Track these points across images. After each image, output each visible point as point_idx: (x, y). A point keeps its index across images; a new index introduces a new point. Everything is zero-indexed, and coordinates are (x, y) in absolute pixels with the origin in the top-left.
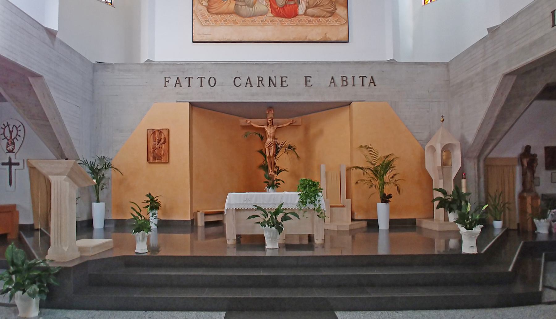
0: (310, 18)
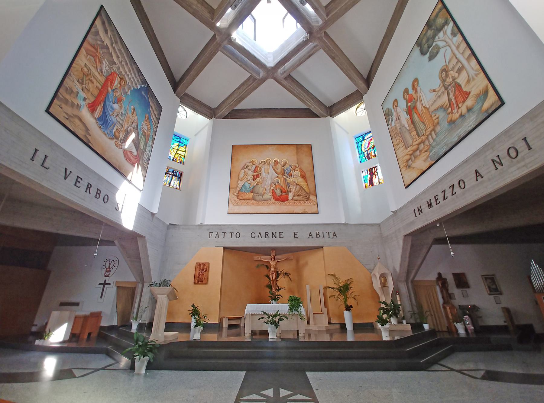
0: (295, 201)
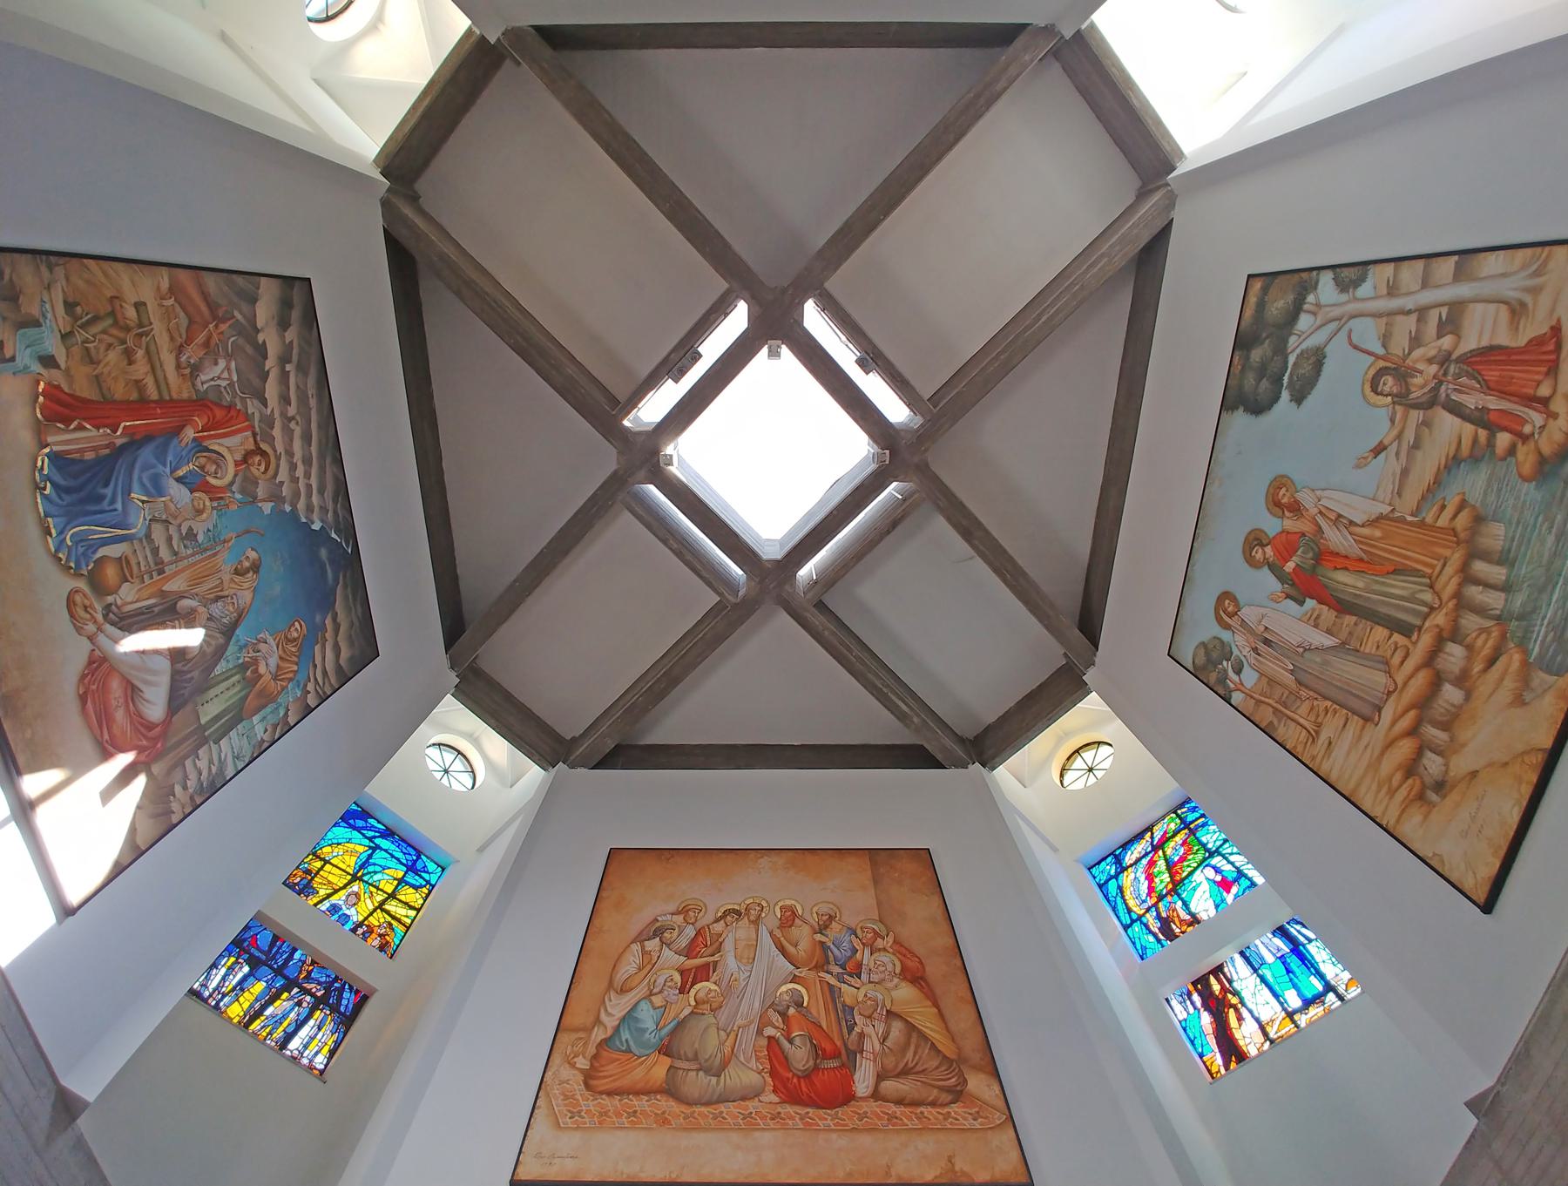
0: (893, 1108)
